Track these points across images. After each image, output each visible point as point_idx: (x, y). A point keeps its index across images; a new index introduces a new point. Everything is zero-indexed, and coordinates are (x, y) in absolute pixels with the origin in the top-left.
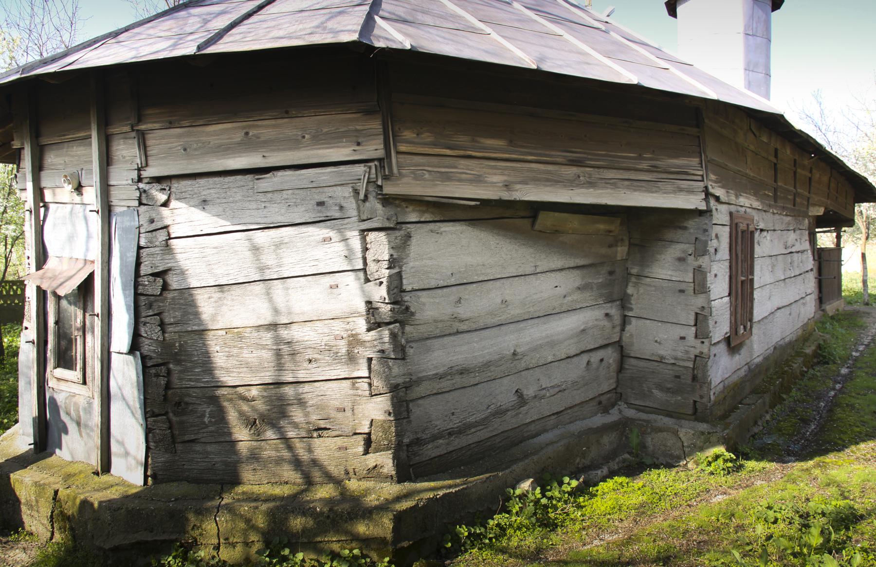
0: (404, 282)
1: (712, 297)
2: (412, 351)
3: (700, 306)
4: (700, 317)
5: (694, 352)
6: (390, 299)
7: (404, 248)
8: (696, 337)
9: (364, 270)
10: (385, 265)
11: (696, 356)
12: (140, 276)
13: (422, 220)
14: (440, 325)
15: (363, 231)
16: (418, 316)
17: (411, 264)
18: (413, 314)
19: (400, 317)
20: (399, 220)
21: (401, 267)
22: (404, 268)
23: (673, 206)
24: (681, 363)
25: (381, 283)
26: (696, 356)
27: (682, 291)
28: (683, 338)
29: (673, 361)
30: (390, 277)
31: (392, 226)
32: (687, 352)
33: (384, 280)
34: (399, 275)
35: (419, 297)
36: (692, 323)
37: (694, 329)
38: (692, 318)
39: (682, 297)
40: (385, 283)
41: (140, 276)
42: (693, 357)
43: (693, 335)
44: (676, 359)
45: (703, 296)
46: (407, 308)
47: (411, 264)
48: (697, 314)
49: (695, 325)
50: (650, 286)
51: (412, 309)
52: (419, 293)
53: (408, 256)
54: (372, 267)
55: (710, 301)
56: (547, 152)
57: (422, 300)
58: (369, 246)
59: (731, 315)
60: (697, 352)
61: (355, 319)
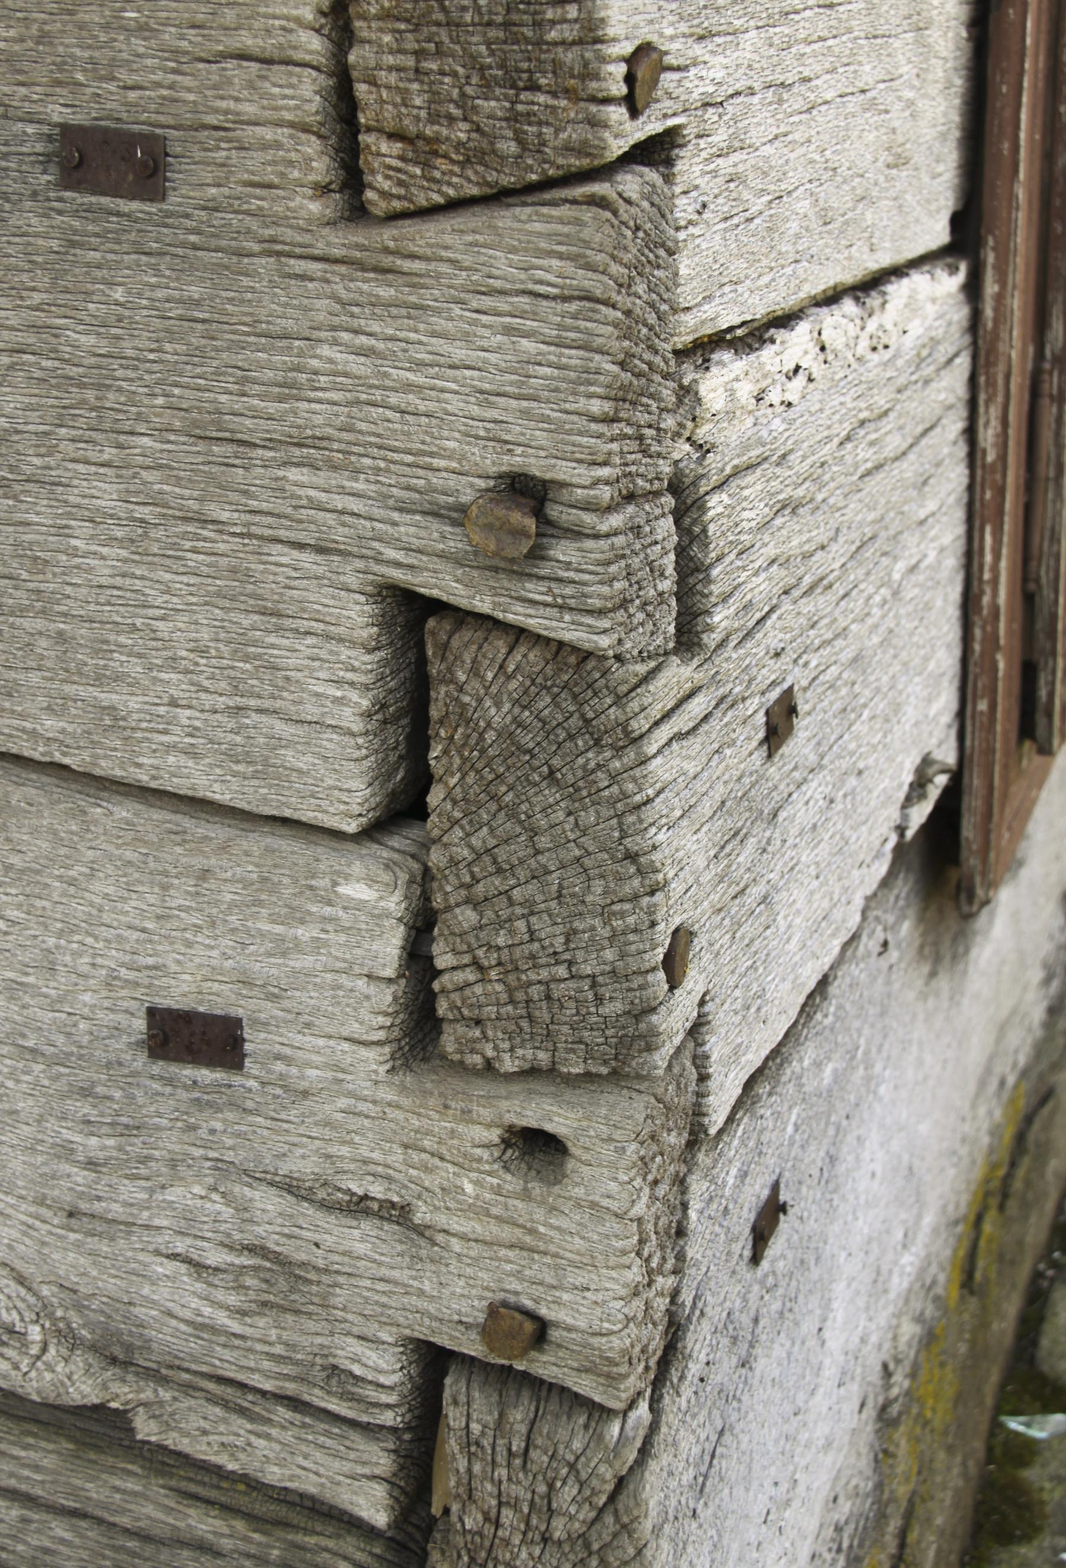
1: (715, 277)
3: (466, 467)
4: (480, 691)
5: (384, 1304)
8: (420, 1029)
11: (432, 1362)
12: (437, 973)
24: (204, 1432)
26: (432, 1362)
27: (112, 160)
28: (196, 1038)
29: (82, 1384)
32: (282, 1279)
36: (344, 785)
37: (369, 893)
38: (337, 681)
39: (128, 282)
41: (437, 973)
42: (383, 1367)
43: (375, 1007)
44: (117, 1353)
45: (519, 244)
48: (411, 617)
49: (403, 806)
55: (658, 364)
56: (1005, 551)
59: (976, 514)
60: (452, 1302)
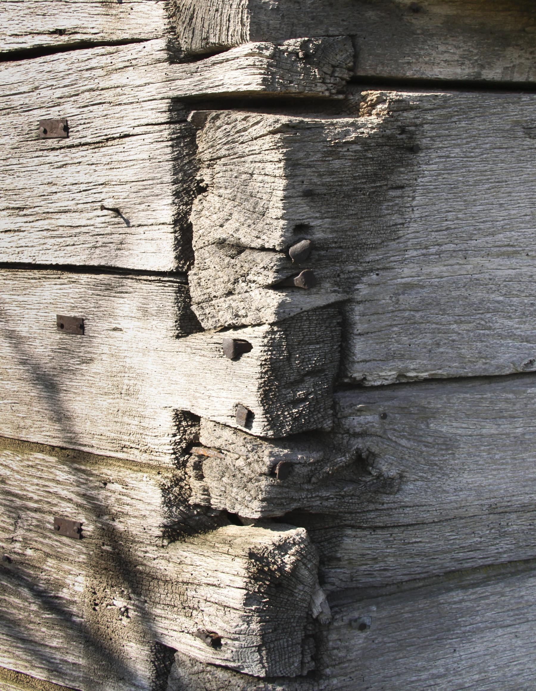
0: (360, 348)
2: (359, 640)
6: (272, 422)
7: (376, 198)
9: (179, 276)
10: (263, 269)
13: (493, 74)
14: (516, 524)
15: (181, 106)
16: (411, 492)
17: (407, 273)
18: (387, 485)
19: (324, 499)
20: (368, 69)
21: (348, 285)
22: (363, 290)
23: (140, 269)
25: (240, 349)
30: (284, 321)
31: (321, 90)
33: (255, 336)
34: (338, 321)
35: (427, 415)
40: (257, 353)
46: (362, 462)
47: (407, 273)
50: (168, 141)
51: (387, 467)
52: (432, 399)
53: (391, 233)
54: (210, 273)
57: (445, 428)
58: (205, 175)
61: (127, 474)
